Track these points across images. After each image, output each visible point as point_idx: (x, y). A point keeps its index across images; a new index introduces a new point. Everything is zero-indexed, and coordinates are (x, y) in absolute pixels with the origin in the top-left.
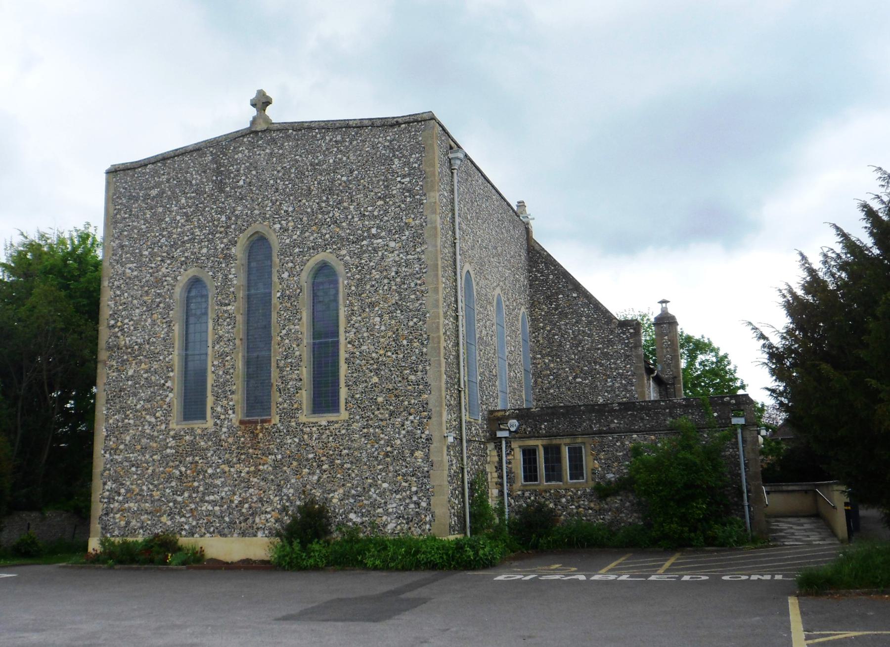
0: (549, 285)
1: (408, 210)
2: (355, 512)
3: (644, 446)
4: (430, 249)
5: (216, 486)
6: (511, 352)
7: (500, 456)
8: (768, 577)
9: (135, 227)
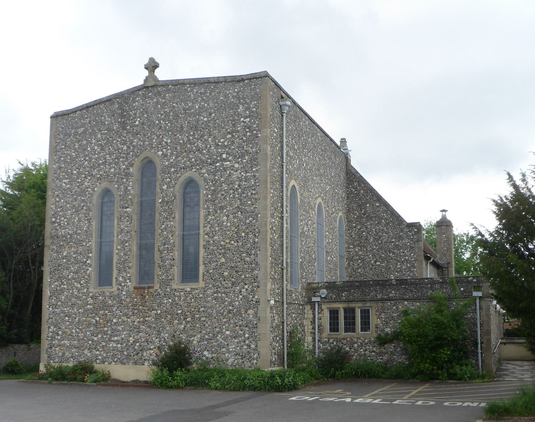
0: (361, 199)
1: (248, 141)
2: (208, 351)
3: (412, 310)
4: (262, 169)
5: (118, 331)
6: (328, 243)
7: (314, 314)
8: (475, 404)
9: (68, 155)
